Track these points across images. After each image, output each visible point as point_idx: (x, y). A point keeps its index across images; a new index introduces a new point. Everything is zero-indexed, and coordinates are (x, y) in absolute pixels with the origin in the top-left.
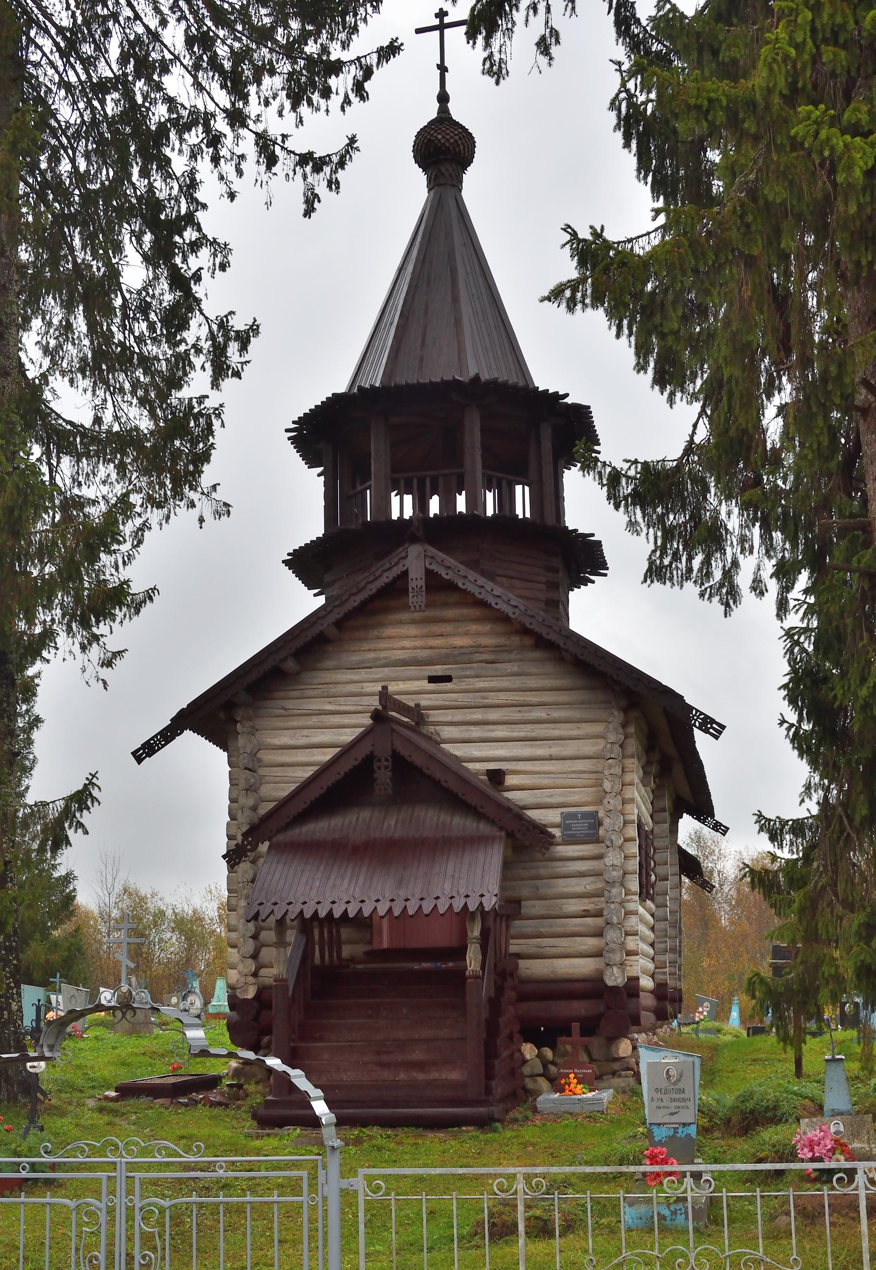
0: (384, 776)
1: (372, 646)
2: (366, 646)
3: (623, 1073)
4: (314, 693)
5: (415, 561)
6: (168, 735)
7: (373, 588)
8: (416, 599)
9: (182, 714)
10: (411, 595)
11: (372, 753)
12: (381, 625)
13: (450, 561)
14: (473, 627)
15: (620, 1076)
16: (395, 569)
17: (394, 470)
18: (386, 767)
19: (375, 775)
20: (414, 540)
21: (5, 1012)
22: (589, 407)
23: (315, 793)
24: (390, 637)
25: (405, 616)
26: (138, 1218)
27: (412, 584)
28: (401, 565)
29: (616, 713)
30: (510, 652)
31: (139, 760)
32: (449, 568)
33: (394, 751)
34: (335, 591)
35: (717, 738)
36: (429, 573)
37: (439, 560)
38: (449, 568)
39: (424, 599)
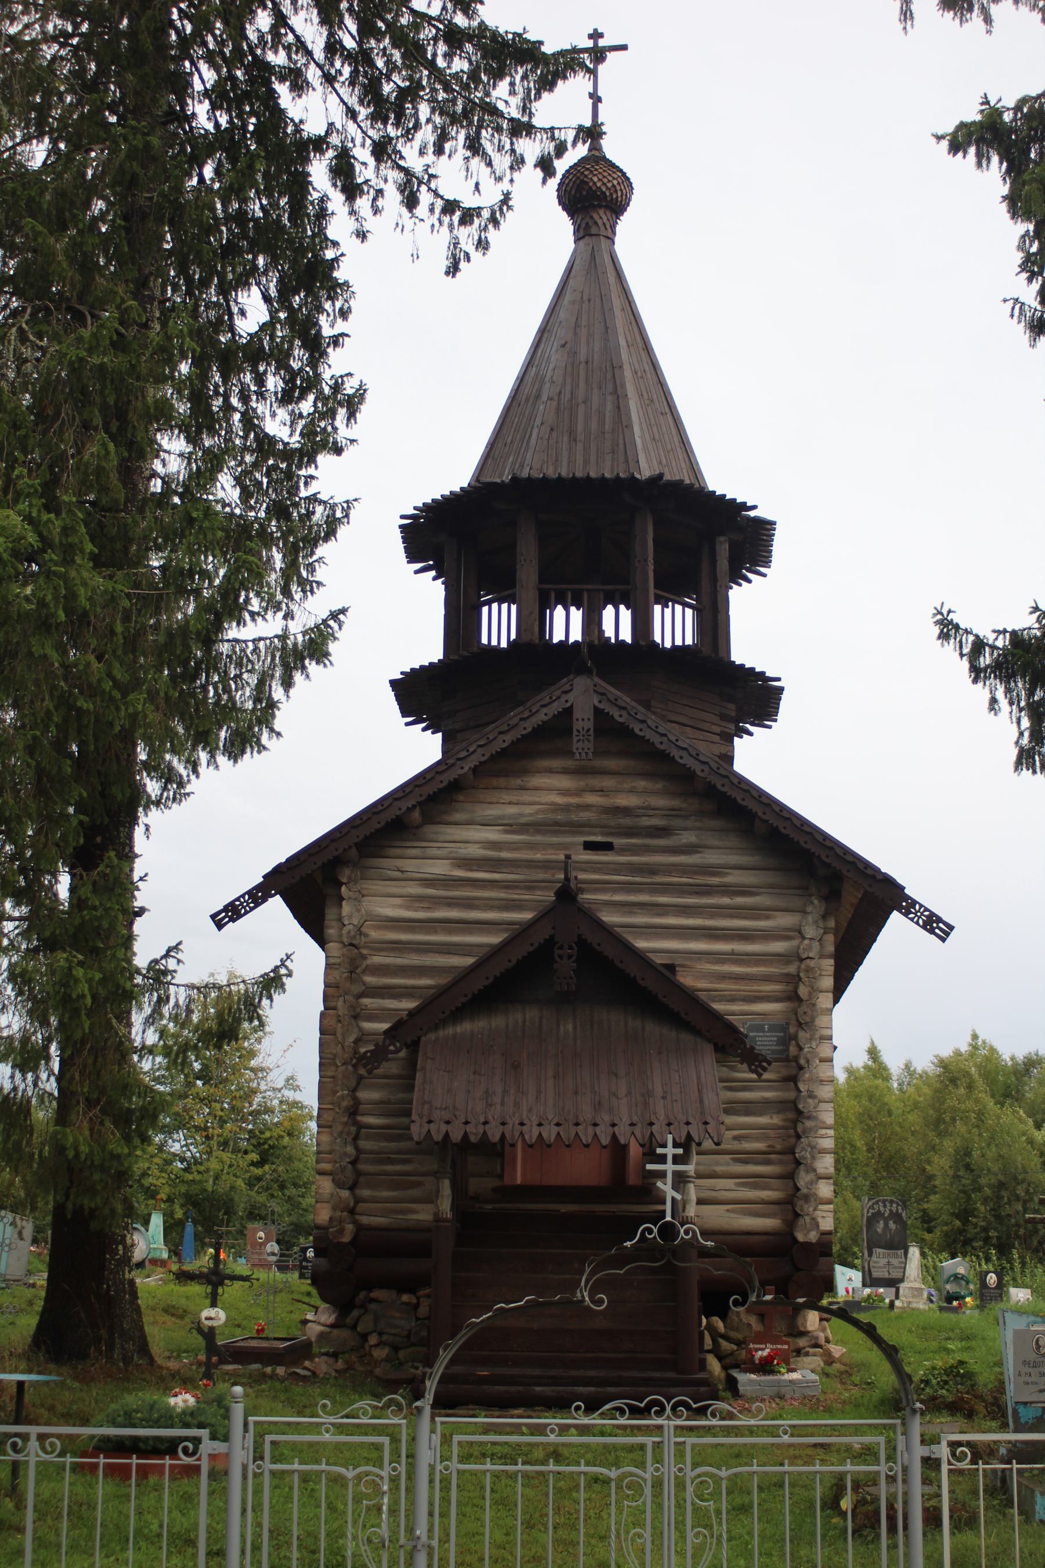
0: (566, 965)
1: (513, 798)
2: (506, 797)
3: (811, 1350)
4: (435, 852)
5: (582, 696)
6: (257, 896)
7: (529, 726)
8: (582, 745)
9: (277, 870)
10: (575, 739)
11: (552, 937)
12: (525, 772)
13: (626, 700)
14: (642, 784)
15: (807, 1354)
16: (555, 704)
17: (541, 581)
18: (570, 957)
19: (556, 966)
20: (583, 670)
21: (120, 1247)
22: (774, 523)
23: (480, 983)
24: (537, 789)
25: (557, 763)
26: (690, 1489)
27: (577, 725)
28: (563, 699)
29: (816, 902)
30: (686, 817)
31: (220, 926)
32: (624, 708)
33: (579, 936)
34: (708, 749)
35: (943, 940)
36: (597, 711)
37: (612, 698)
38: (624, 708)
39: (591, 746)
